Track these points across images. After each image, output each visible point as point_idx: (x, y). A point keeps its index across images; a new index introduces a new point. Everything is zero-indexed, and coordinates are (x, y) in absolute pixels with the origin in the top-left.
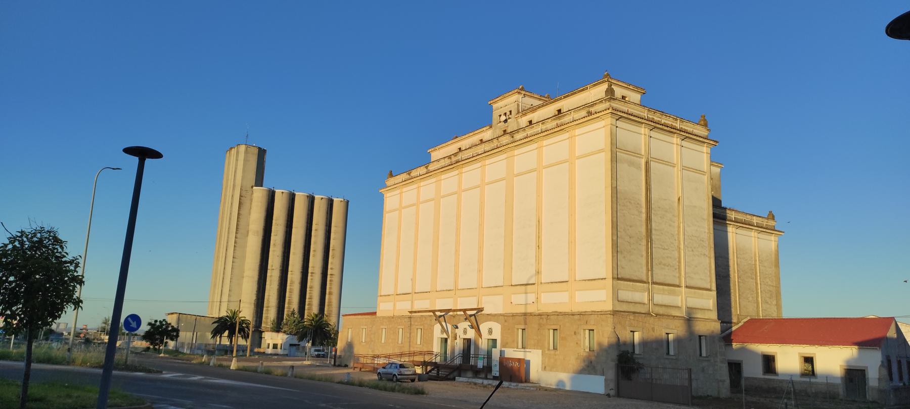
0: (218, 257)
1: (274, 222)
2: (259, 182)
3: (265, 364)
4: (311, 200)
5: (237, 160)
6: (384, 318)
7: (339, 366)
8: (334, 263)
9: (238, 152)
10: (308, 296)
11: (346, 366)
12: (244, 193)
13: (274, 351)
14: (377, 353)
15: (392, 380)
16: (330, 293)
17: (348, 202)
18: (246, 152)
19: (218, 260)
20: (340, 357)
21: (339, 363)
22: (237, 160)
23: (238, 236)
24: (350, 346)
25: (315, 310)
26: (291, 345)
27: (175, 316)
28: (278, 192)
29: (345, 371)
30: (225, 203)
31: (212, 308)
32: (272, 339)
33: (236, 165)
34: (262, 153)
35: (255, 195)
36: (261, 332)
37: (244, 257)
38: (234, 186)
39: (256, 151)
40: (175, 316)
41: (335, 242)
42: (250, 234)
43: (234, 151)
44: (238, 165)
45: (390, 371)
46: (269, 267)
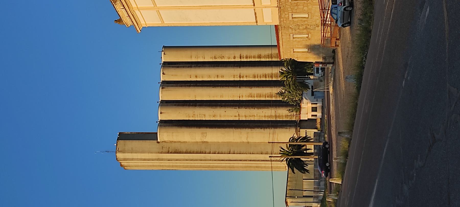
0: (230, 167)
1: (191, 119)
2: (153, 136)
3: (334, 155)
4: (166, 84)
5: (132, 159)
6: (280, 17)
7: (334, 58)
8: (228, 56)
9: (125, 159)
10: (264, 79)
11: (334, 51)
12: (165, 150)
13: (319, 110)
14: (319, 22)
15: (351, 13)
16: (259, 57)
17: (164, 47)
18: (123, 152)
19: (233, 167)
20: (324, 58)
21: (331, 57)
22: (132, 159)
23: (208, 151)
24: (312, 48)
25: (275, 90)
26: (313, 95)
27: (289, 200)
28: (161, 117)
29: (340, 55)
30: (176, 166)
31: (280, 168)
32: (307, 110)
33: (138, 159)
34: (123, 137)
35: (166, 139)
36: (301, 121)
37: (228, 143)
38: (158, 160)
39: (121, 142)
40: (289, 200)
41: (208, 57)
42: (205, 140)
43: (124, 163)
44: (137, 158)
45: (339, 14)
46: (237, 119)
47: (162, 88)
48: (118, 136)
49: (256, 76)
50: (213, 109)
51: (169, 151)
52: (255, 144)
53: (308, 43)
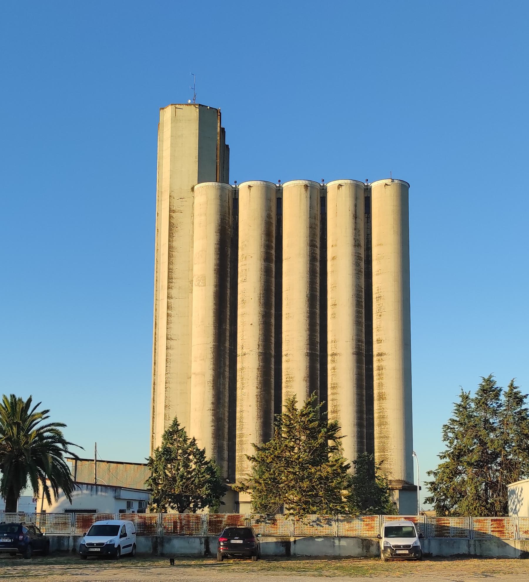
18: (175, 119)
47: (306, 186)
48: (209, 105)
49: (335, 391)
50: (257, 299)
51: (174, 211)
52: (186, 393)
53: (509, 518)
